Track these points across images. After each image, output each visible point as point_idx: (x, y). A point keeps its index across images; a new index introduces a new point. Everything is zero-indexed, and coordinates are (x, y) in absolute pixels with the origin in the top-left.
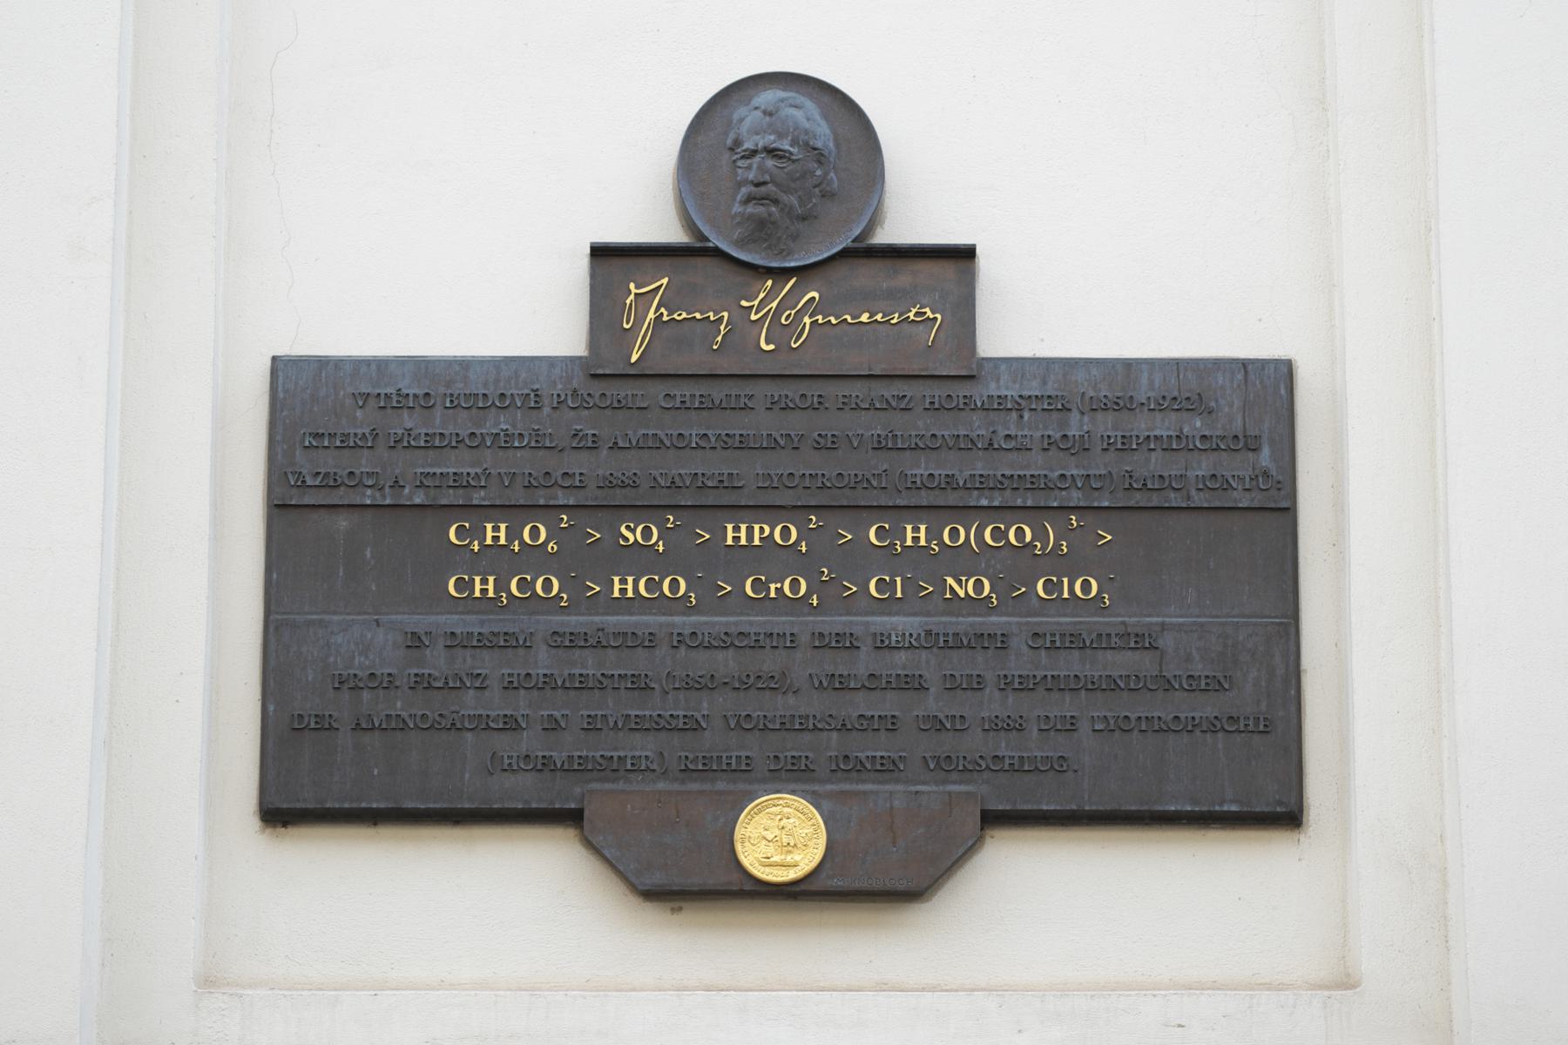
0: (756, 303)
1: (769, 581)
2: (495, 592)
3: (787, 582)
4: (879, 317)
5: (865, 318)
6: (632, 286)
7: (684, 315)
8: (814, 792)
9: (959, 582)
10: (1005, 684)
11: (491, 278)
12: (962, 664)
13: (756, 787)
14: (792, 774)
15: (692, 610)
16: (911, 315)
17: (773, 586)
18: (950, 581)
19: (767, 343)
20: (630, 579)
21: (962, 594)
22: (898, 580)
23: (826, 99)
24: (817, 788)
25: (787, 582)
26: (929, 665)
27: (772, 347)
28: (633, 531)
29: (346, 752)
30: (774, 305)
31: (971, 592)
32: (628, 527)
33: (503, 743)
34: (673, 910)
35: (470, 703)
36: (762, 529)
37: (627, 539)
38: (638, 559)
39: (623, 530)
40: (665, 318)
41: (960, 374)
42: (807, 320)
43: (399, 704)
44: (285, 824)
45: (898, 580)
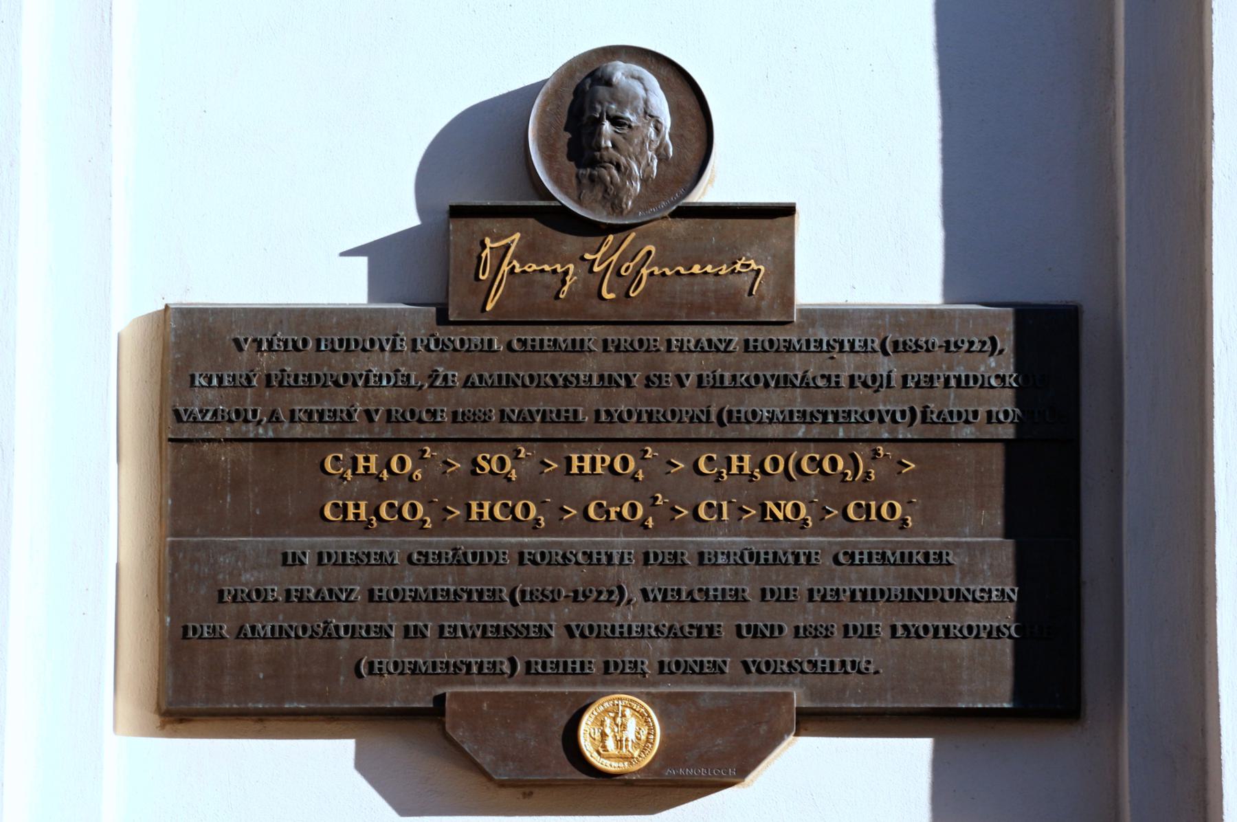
0: (599, 256)
1: (610, 505)
2: (367, 514)
3: (626, 505)
4: (709, 269)
5: (696, 269)
6: (487, 241)
7: (534, 267)
8: (648, 694)
9: (778, 506)
10: (738, 596)
11: (312, 233)
12: (776, 578)
13: (599, 689)
14: (617, 673)
15: (430, 533)
16: (738, 267)
17: (613, 510)
18: (770, 505)
19: (609, 292)
20: (487, 505)
21: (780, 516)
22: (725, 504)
23: (664, 71)
24: (653, 690)
25: (626, 505)
26: (748, 580)
27: (612, 296)
28: (489, 462)
29: (215, 662)
30: (615, 257)
31: (790, 516)
32: (484, 458)
33: (368, 651)
34: (525, 795)
35: (341, 617)
36: (603, 460)
37: (482, 469)
38: (501, 487)
39: (479, 459)
40: (517, 270)
41: (767, 314)
42: (645, 272)
43: (281, 617)
44: (181, 721)
45: (725, 504)
